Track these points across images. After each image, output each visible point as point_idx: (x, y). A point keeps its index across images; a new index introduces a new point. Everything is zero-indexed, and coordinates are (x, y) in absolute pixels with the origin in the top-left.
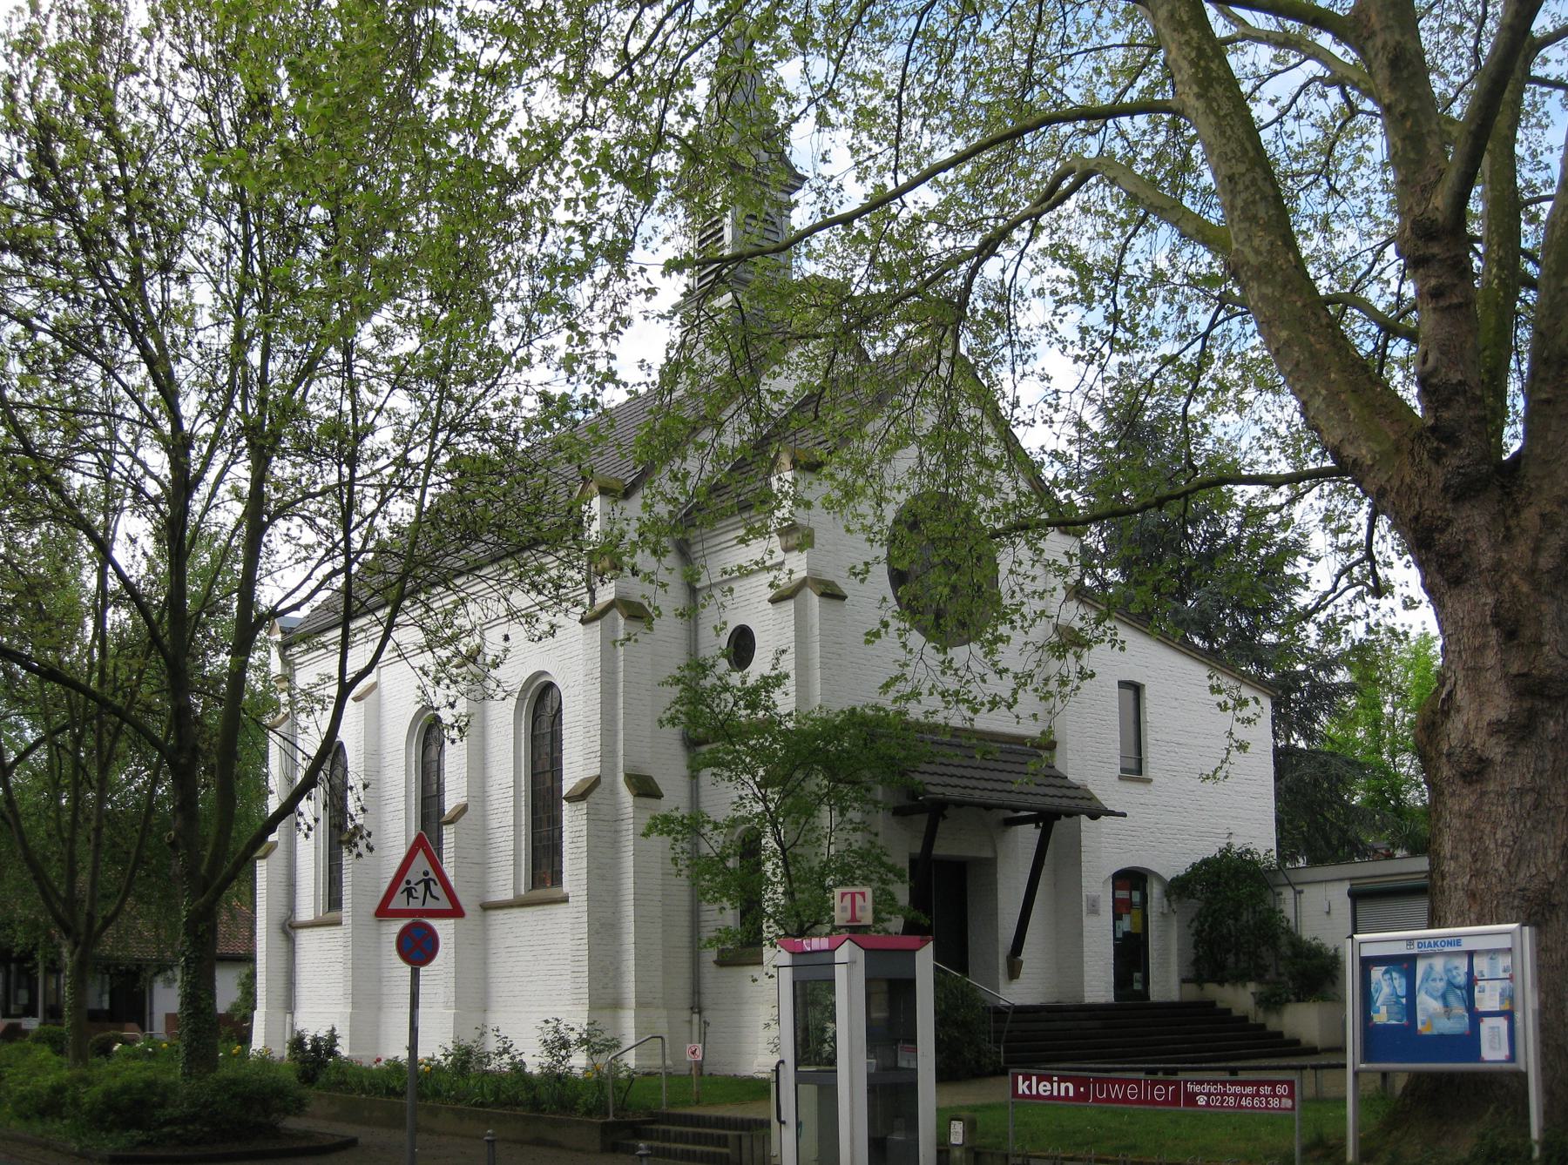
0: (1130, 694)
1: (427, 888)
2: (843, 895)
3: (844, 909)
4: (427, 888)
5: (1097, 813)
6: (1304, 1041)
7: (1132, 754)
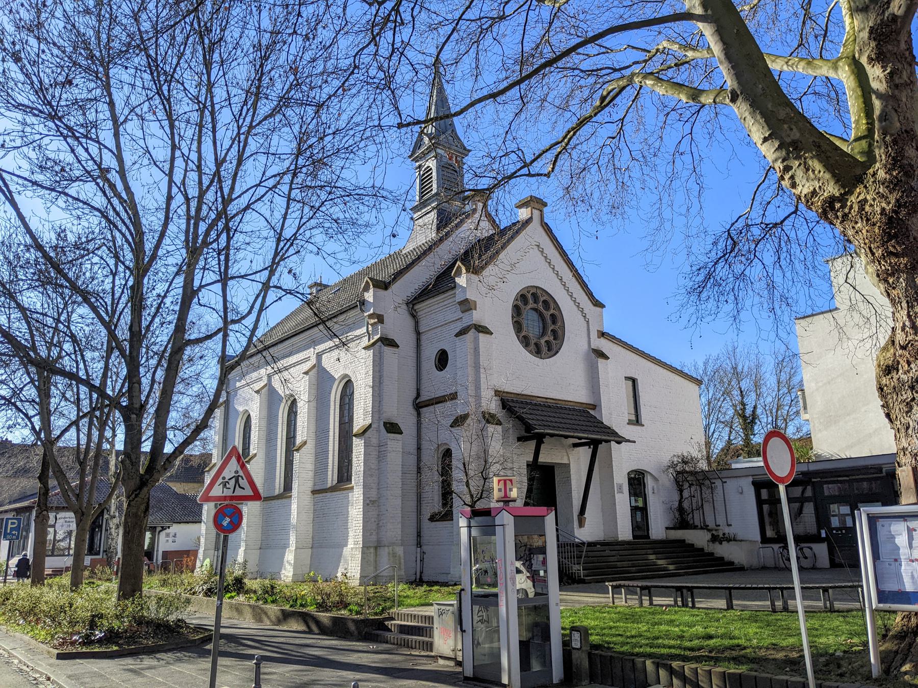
0: (630, 383)
1: (237, 481)
2: (499, 481)
3: (500, 490)
4: (237, 481)
5: (620, 440)
6: (736, 562)
7: (633, 412)
